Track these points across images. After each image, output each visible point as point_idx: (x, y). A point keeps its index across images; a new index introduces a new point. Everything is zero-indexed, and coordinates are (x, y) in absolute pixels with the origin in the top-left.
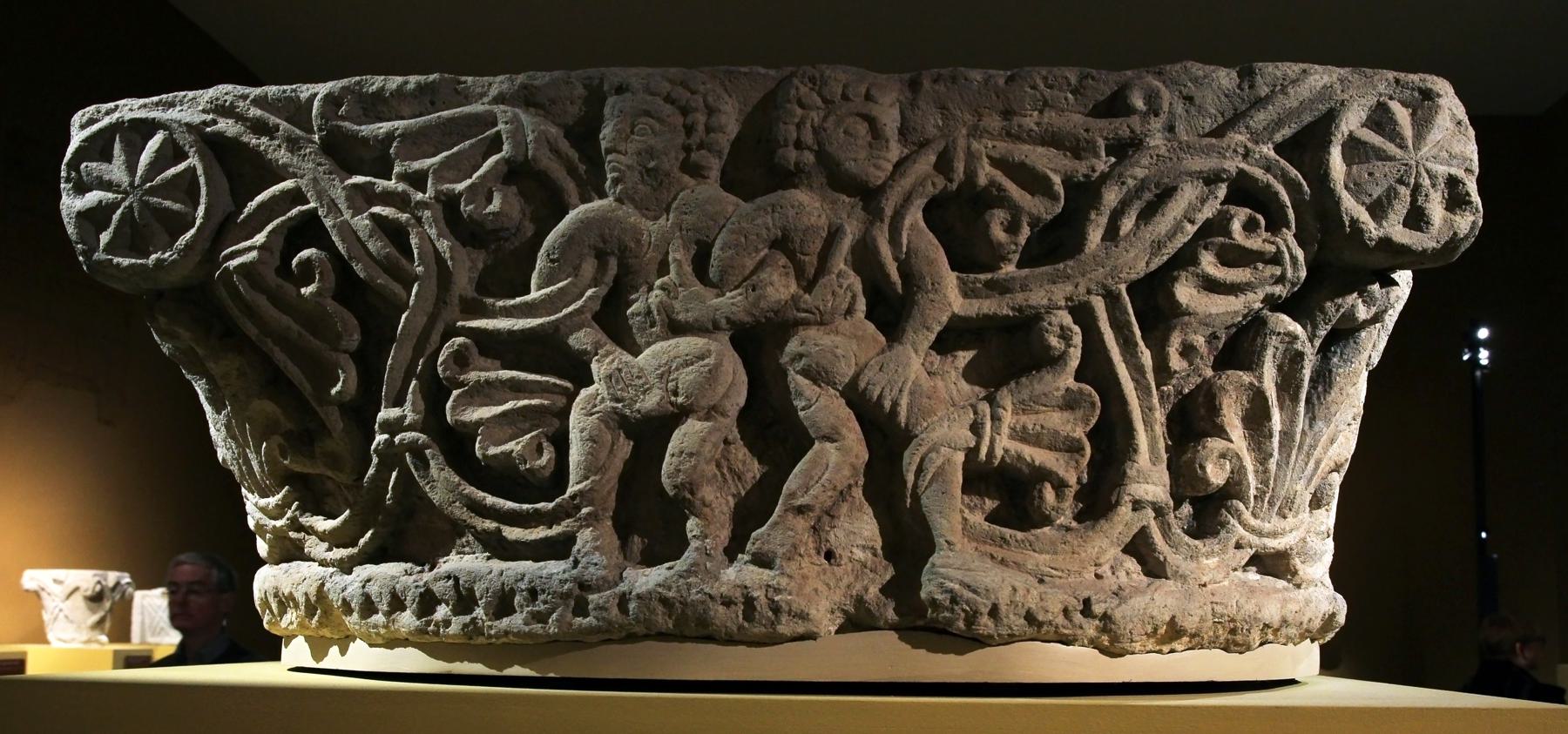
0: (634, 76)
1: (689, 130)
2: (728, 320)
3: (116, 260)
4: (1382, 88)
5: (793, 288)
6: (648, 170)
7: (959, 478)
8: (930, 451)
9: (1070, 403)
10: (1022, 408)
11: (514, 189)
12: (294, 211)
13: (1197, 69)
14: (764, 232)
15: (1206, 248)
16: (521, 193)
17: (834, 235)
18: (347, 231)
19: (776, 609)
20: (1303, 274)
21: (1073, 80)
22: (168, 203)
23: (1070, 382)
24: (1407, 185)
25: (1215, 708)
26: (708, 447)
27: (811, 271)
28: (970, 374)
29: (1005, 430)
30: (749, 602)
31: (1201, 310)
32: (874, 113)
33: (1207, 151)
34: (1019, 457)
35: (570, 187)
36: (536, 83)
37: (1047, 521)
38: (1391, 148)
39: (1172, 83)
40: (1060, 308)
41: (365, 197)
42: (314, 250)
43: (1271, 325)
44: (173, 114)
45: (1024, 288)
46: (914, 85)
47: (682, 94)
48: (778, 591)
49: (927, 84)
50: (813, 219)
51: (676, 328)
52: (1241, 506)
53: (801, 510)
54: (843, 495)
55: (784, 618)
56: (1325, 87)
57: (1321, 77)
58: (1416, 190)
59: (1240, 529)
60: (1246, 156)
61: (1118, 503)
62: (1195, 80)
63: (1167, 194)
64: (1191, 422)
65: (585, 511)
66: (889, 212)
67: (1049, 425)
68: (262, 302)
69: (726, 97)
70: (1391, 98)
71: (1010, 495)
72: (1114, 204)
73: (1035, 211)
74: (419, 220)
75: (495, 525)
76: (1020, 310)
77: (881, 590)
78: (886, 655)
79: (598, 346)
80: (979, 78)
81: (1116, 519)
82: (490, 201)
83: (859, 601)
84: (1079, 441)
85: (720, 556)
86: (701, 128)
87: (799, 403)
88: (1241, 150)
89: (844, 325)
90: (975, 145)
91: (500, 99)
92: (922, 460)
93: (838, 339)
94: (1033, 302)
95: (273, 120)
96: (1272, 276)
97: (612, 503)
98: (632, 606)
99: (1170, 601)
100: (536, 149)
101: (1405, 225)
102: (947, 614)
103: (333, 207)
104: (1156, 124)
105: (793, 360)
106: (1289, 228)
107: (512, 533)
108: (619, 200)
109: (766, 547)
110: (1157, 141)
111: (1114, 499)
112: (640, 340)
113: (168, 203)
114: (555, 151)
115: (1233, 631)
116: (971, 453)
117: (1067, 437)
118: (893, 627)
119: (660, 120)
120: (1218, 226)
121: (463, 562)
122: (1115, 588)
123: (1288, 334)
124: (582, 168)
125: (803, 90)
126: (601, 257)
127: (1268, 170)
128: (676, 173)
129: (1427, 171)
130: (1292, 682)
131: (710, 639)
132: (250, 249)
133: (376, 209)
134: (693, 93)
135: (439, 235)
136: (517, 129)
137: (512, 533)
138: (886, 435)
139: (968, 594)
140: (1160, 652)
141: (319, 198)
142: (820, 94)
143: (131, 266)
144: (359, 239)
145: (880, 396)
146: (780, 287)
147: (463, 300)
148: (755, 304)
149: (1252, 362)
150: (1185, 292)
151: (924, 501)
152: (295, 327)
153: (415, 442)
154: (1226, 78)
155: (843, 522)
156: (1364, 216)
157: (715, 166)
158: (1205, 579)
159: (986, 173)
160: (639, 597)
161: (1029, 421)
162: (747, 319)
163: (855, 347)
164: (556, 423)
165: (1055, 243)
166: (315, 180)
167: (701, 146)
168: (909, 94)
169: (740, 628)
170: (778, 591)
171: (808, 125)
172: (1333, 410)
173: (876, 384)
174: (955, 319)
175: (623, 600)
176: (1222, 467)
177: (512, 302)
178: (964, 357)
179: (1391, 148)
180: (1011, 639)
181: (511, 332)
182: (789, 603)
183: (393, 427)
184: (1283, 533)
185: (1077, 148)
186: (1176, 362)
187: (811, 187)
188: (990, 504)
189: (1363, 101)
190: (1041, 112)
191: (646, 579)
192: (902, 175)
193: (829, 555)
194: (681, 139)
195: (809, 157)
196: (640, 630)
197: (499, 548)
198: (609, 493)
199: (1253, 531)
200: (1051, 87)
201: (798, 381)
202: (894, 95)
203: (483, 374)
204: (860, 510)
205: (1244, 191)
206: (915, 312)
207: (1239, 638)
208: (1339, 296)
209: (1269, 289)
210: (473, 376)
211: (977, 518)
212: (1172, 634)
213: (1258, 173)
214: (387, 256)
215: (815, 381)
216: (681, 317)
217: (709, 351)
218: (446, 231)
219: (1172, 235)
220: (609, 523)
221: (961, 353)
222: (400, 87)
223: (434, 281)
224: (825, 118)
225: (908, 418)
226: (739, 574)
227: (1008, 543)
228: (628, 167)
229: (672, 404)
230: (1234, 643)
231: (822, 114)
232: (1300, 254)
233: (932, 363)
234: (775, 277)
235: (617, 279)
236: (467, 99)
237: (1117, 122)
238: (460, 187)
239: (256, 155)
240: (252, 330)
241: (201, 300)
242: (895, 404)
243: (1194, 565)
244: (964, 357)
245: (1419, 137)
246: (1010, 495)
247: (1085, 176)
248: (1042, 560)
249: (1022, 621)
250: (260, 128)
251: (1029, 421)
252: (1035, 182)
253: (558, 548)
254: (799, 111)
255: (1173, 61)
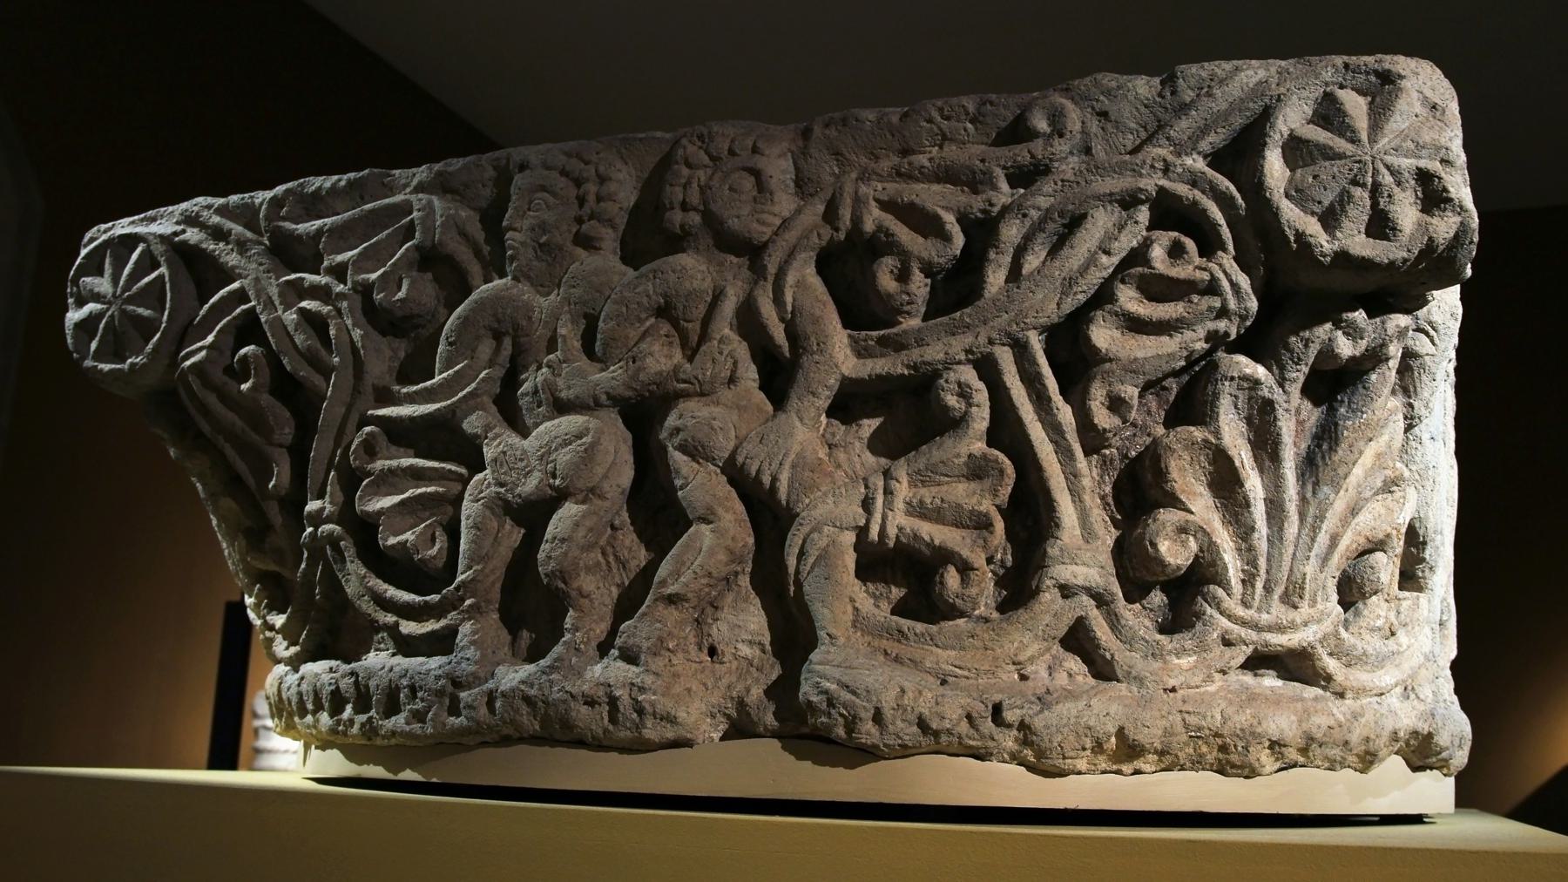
0: (531, 153)
1: (581, 201)
2: (607, 394)
3: (101, 366)
4: (1328, 75)
5: (678, 356)
6: (541, 245)
7: (850, 559)
8: (813, 530)
9: (977, 470)
10: (920, 479)
11: (429, 275)
12: (238, 310)
13: (1109, 80)
14: (645, 300)
15: (1123, 281)
16: (436, 279)
17: (718, 296)
18: (278, 324)
19: (640, 711)
20: (1253, 304)
21: (971, 108)
22: (141, 310)
23: (979, 447)
24: (1363, 185)
25: (1190, 841)
26: (581, 532)
27: (694, 339)
28: (876, 444)
29: (899, 504)
30: (613, 702)
31: (1123, 354)
32: (759, 166)
33: (1119, 169)
34: (916, 537)
35: (475, 269)
36: (451, 169)
37: (953, 612)
38: (1340, 144)
39: (1081, 99)
40: (959, 363)
41: (298, 291)
42: (252, 347)
43: (1223, 369)
44: (155, 228)
45: (920, 343)
46: (806, 134)
47: (575, 166)
48: (642, 689)
49: (817, 130)
50: (696, 284)
51: (562, 407)
52: (1220, 592)
53: (672, 600)
54: (728, 581)
55: (649, 723)
56: (1260, 83)
57: (1254, 73)
58: (1376, 190)
59: (1224, 622)
60: (1166, 171)
61: (1037, 592)
62: (1108, 93)
63: (1075, 223)
64: (1139, 492)
65: (468, 602)
66: (772, 269)
67: (951, 498)
68: (212, 400)
69: (619, 165)
70: (1342, 87)
71: (910, 577)
72: (1017, 240)
73: (925, 255)
74: (339, 311)
75: (395, 619)
76: (915, 367)
77: (766, 692)
78: (770, 768)
79: (488, 428)
80: (871, 117)
81: (1037, 607)
82: (399, 289)
83: (741, 704)
84: (986, 515)
85: (592, 651)
86: (591, 198)
87: (678, 482)
88: (1159, 165)
89: (726, 394)
90: (863, 189)
91: (420, 188)
92: (804, 541)
93: (716, 410)
94: (928, 358)
95: (229, 224)
96: (1210, 309)
97: (496, 594)
98: (498, 704)
99: (1114, 708)
100: (442, 233)
101: (1368, 234)
102: (824, 719)
103: (269, 305)
104: (1061, 147)
105: (671, 435)
106: (1225, 250)
107: (408, 627)
108: (515, 278)
109: (631, 642)
110: (1069, 166)
111: (1034, 584)
112: (529, 422)
113: (141, 310)
114: (463, 234)
115: (1223, 748)
116: (862, 532)
117: (972, 512)
118: (774, 735)
119: (554, 194)
120: (1138, 256)
121: (379, 660)
122: (1041, 691)
123: (1245, 378)
124: (486, 249)
125: (691, 149)
126: (498, 336)
127: (1194, 184)
128: (569, 246)
129: (1388, 167)
130: (286, 771)
131: (580, 743)
132: (201, 349)
133: (304, 304)
134: (587, 163)
135: (354, 325)
136: (427, 215)
137: (408, 627)
138: (770, 516)
139: (846, 696)
140: (1118, 772)
141: (258, 297)
142: (707, 153)
143: (111, 371)
144: (288, 333)
145: (758, 471)
146: (661, 358)
147: (376, 388)
148: (635, 377)
149: (1205, 415)
150: (1103, 335)
151: (806, 588)
152: (239, 423)
153: (331, 534)
154: (1144, 86)
155: (726, 614)
156: (1313, 227)
157: (610, 239)
158: (1171, 683)
159: (873, 218)
160: (503, 695)
161: (927, 495)
162: (629, 393)
163: (735, 418)
164: (450, 510)
165: (957, 288)
166: (257, 280)
167: (591, 217)
168: (800, 143)
169: (606, 731)
170: (642, 689)
171: (695, 185)
172: (1341, 471)
173: (755, 461)
174: (846, 382)
175: (491, 697)
176: (1184, 544)
177: (415, 388)
178: (870, 425)
179: (1340, 144)
180: (905, 752)
181: (412, 419)
182: (653, 704)
183: (317, 519)
184: (1293, 626)
185: (975, 182)
186: (1103, 418)
187: (697, 251)
188: (897, 593)
189: (1305, 94)
190: (941, 147)
191: (512, 676)
192: (1065, 251)
193: (712, 652)
194: (574, 211)
195: (695, 218)
196: (507, 731)
197: (407, 646)
198: (493, 583)
199: (1244, 623)
200: (948, 118)
201: (678, 458)
202: (785, 144)
203: (388, 462)
204: (746, 600)
205: (1171, 213)
206: (800, 376)
207: (1234, 758)
208: (1304, 328)
209: (1211, 325)
210: (380, 464)
211: (883, 613)
212: (1127, 751)
213: (1182, 189)
214: (309, 348)
215: (693, 457)
216: (563, 395)
217: (587, 429)
218: (363, 320)
219: (1084, 270)
220: (496, 616)
221: (866, 422)
222: (334, 185)
223: (350, 371)
224: (711, 178)
225: (789, 495)
226: (612, 670)
227: (907, 638)
228: (522, 243)
229: (550, 486)
230: (1229, 760)
231: (709, 171)
232: (1244, 281)
233: (833, 435)
234: (656, 347)
235: (513, 359)
236: (391, 190)
237: (1017, 149)
238: (374, 276)
239: (210, 260)
240: (206, 428)
241: (170, 399)
242: (775, 479)
243: (1157, 665)
244: (870, 425)
245: (1376, 127)
246: (910, 577)
247: (984, 211)
248: (944, 658)
249: (915, 729)
250: (219, 234)
251: (927, 495)
252: (928, 225)
253: (442, 643)
254: (685, 171)
255: (1082, 76)
